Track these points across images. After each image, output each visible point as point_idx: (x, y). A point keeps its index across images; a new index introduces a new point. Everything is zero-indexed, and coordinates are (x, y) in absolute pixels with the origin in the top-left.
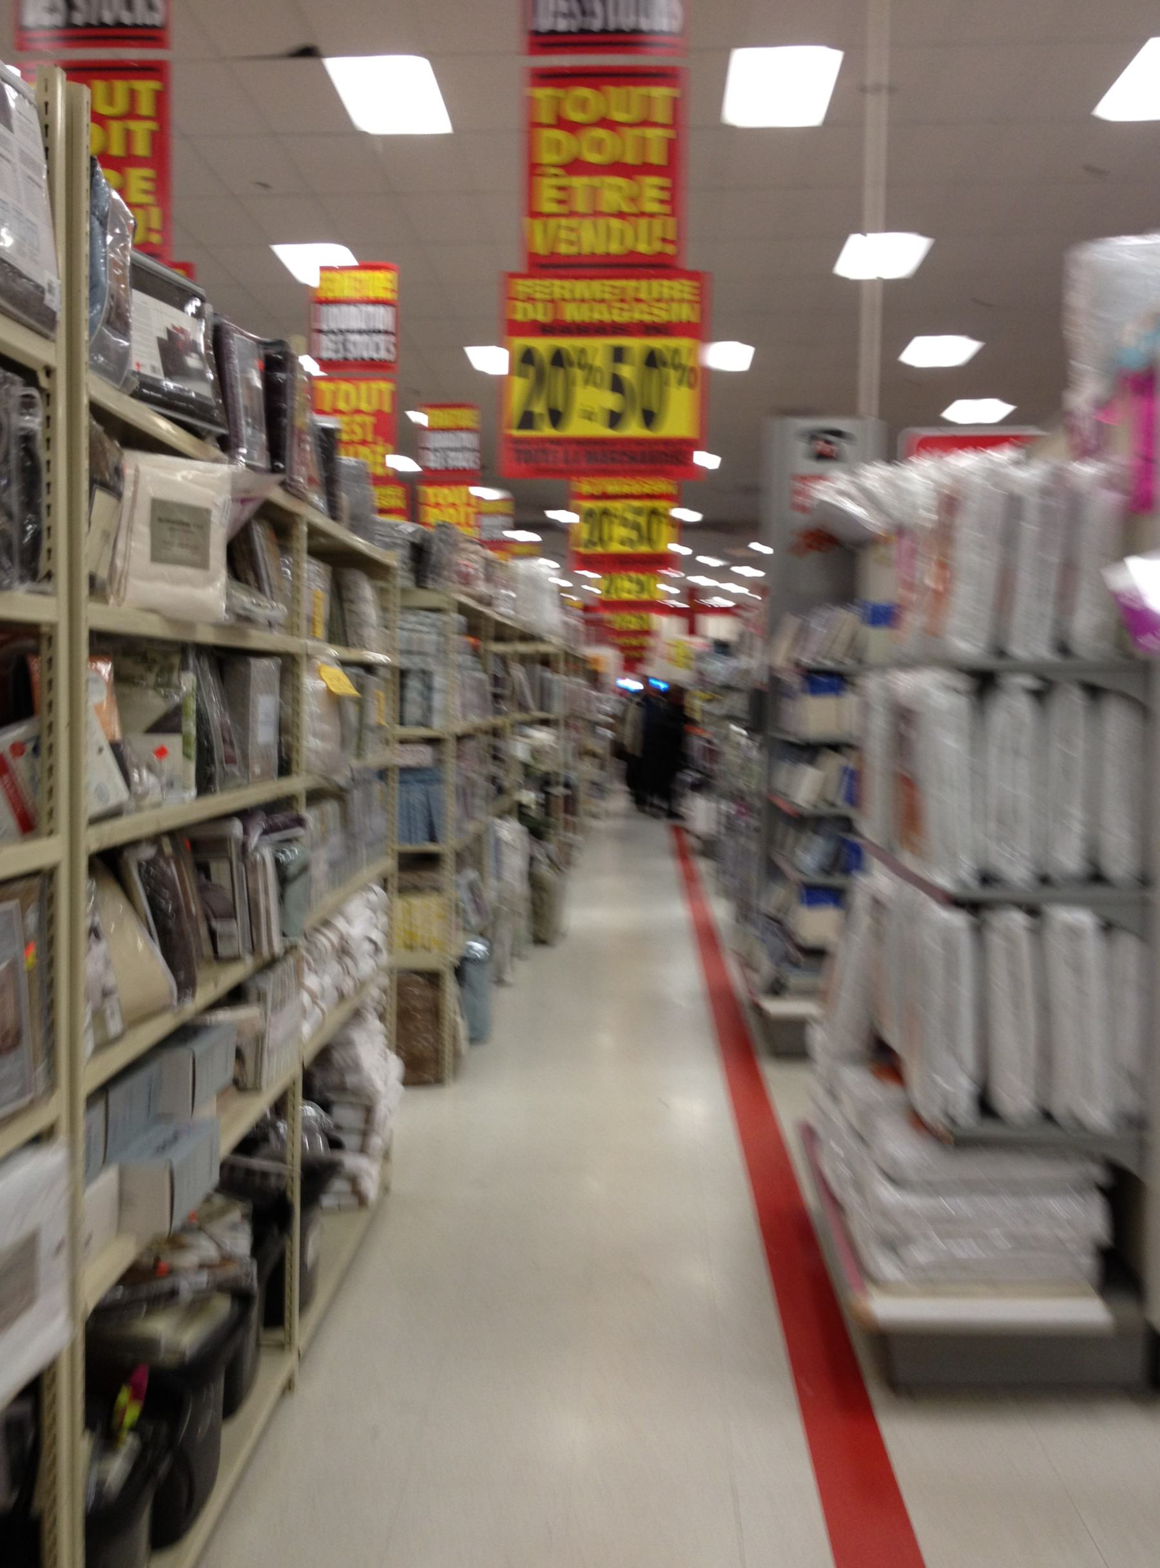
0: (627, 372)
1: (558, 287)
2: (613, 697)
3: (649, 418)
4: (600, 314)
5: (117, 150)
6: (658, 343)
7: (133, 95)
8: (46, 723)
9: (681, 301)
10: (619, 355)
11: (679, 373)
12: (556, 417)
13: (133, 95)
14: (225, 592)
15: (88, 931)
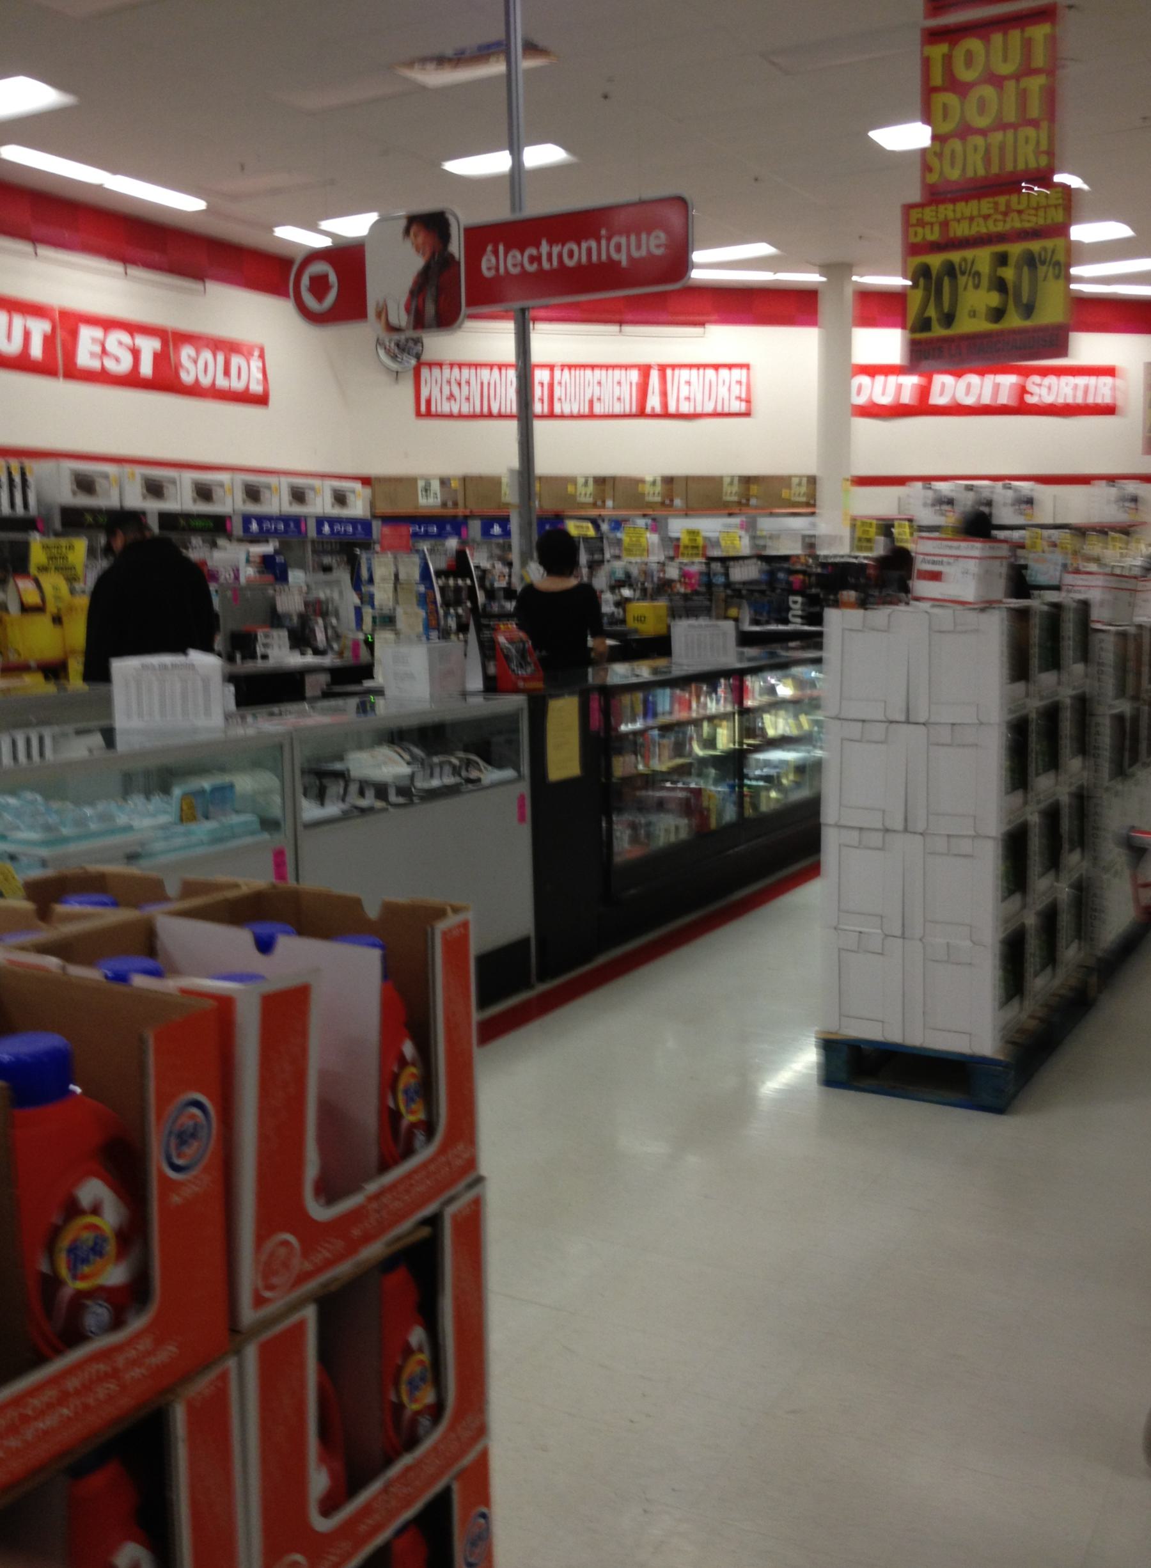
0: (1008, 273)
1: (946, 211)
2: (1099, 581)
3: (1028, 310)
4: (981, 228)
5: (1011, 116)
6: (1035, 246)
7: (27, 335)
8: (741, 586)
9: (1056, 206)
10: (1002, 260)
11: (976, 268)
12: (949, 319)
13: (1028, 44)
14: (817, 486)
15: (376, 315)
